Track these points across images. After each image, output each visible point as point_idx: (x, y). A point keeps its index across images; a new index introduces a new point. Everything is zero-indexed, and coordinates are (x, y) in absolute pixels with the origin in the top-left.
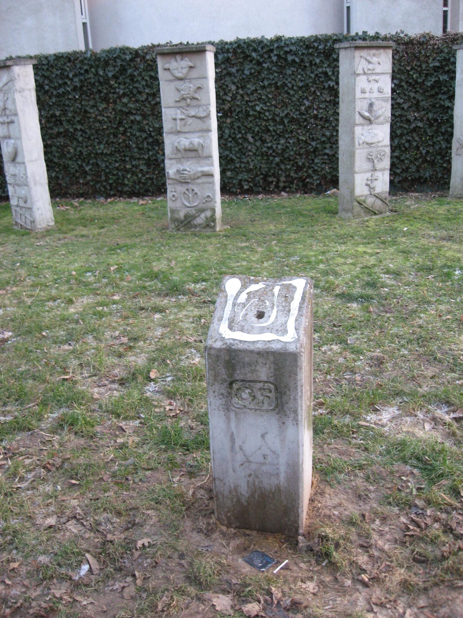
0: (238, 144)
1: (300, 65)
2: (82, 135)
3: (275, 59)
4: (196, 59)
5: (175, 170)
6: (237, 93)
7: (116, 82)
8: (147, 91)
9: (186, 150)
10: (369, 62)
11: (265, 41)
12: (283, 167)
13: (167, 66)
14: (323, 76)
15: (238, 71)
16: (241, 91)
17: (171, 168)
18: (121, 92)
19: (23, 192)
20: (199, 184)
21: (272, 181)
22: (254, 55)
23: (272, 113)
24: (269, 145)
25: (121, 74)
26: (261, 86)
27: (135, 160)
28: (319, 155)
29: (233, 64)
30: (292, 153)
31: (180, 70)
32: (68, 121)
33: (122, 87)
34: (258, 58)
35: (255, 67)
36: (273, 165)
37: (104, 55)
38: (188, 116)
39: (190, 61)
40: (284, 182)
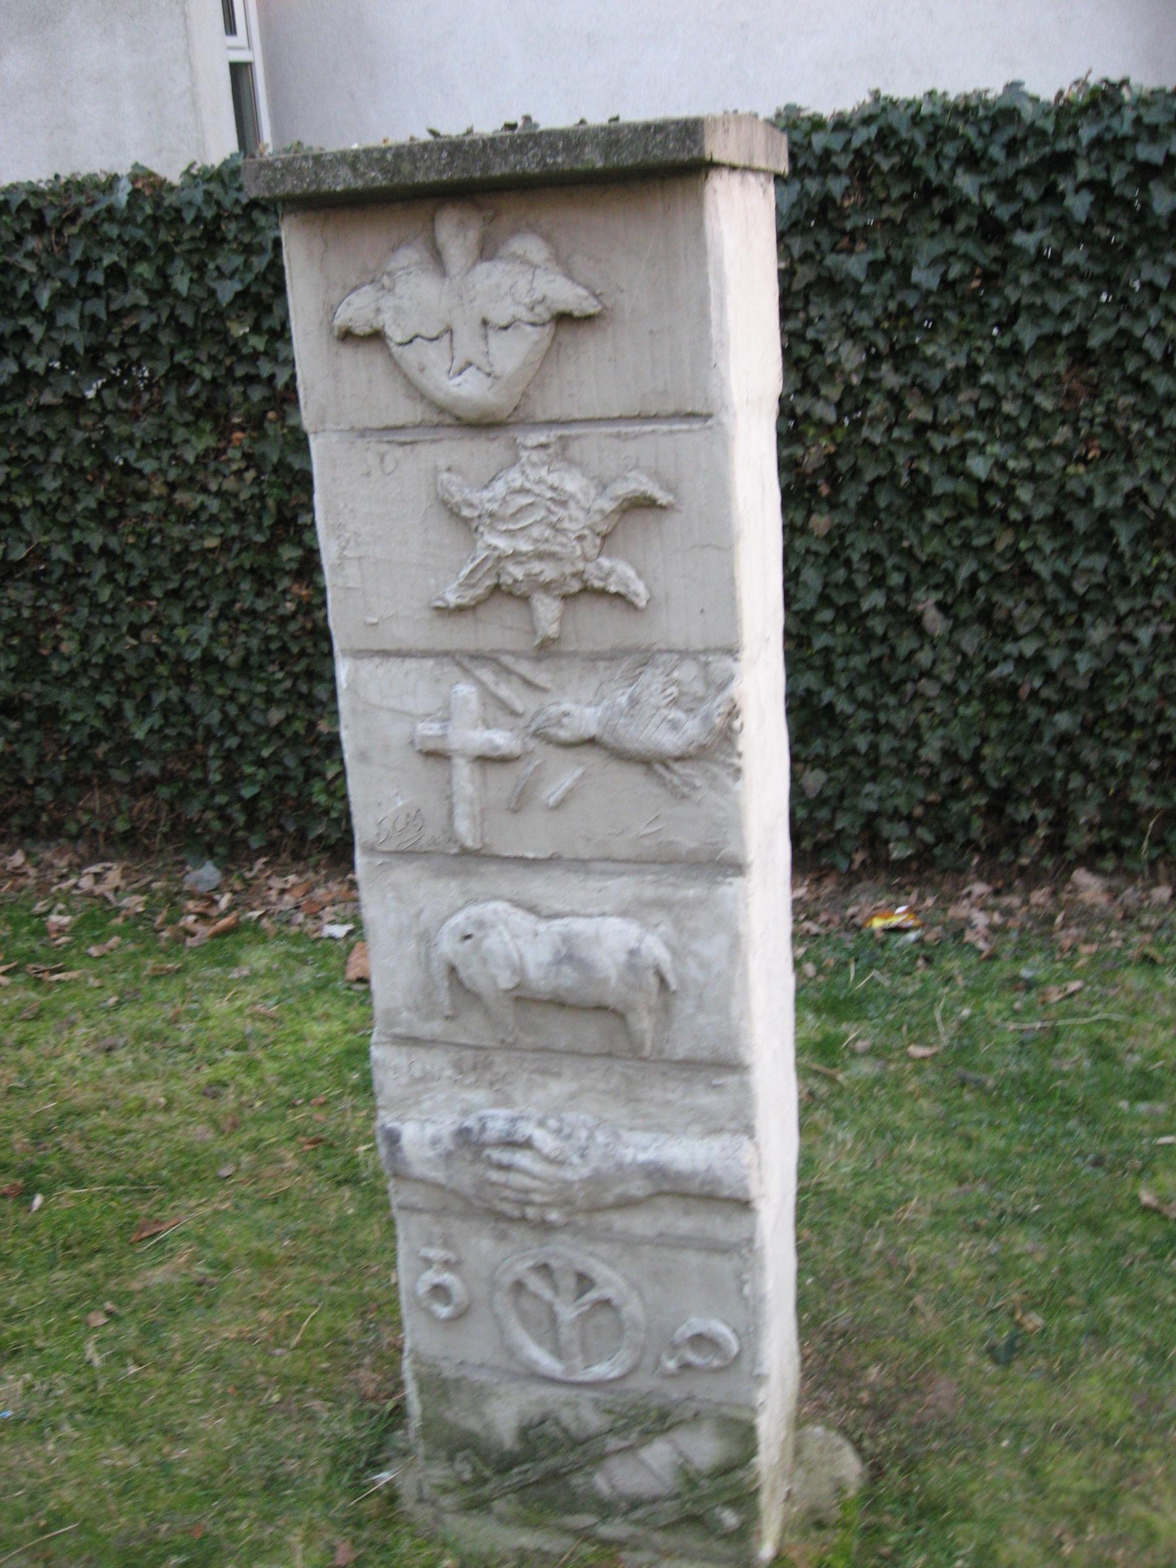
0: (868, 638)
2: (109, 578)
3: (1079, 205)
4: (614, 251)
5: (446, 1125)
6: (867, 382)
7: (256, 329)
9: (523, 998)
11: (1028, 112)
12: (1090, 755)
13: (357, 310)
15: (875, 270)
16: (890, 378)
20: (631, 1243)
21: (1032, 823)
22: (966, 183)
23: (1051, 489)
24: (1029, 648)
26: (999, 352)
29: (852, 236)
30: (1145, 693)
31: (467, 343)
32: (46, 511)
34: (990, 199)
35: (968, 247)
36: (1045, 747)
37: (198, 197)
40: (1091, 827)
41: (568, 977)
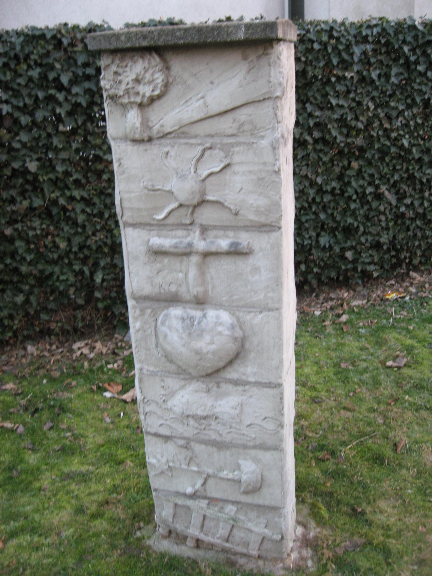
32: (54, 183)
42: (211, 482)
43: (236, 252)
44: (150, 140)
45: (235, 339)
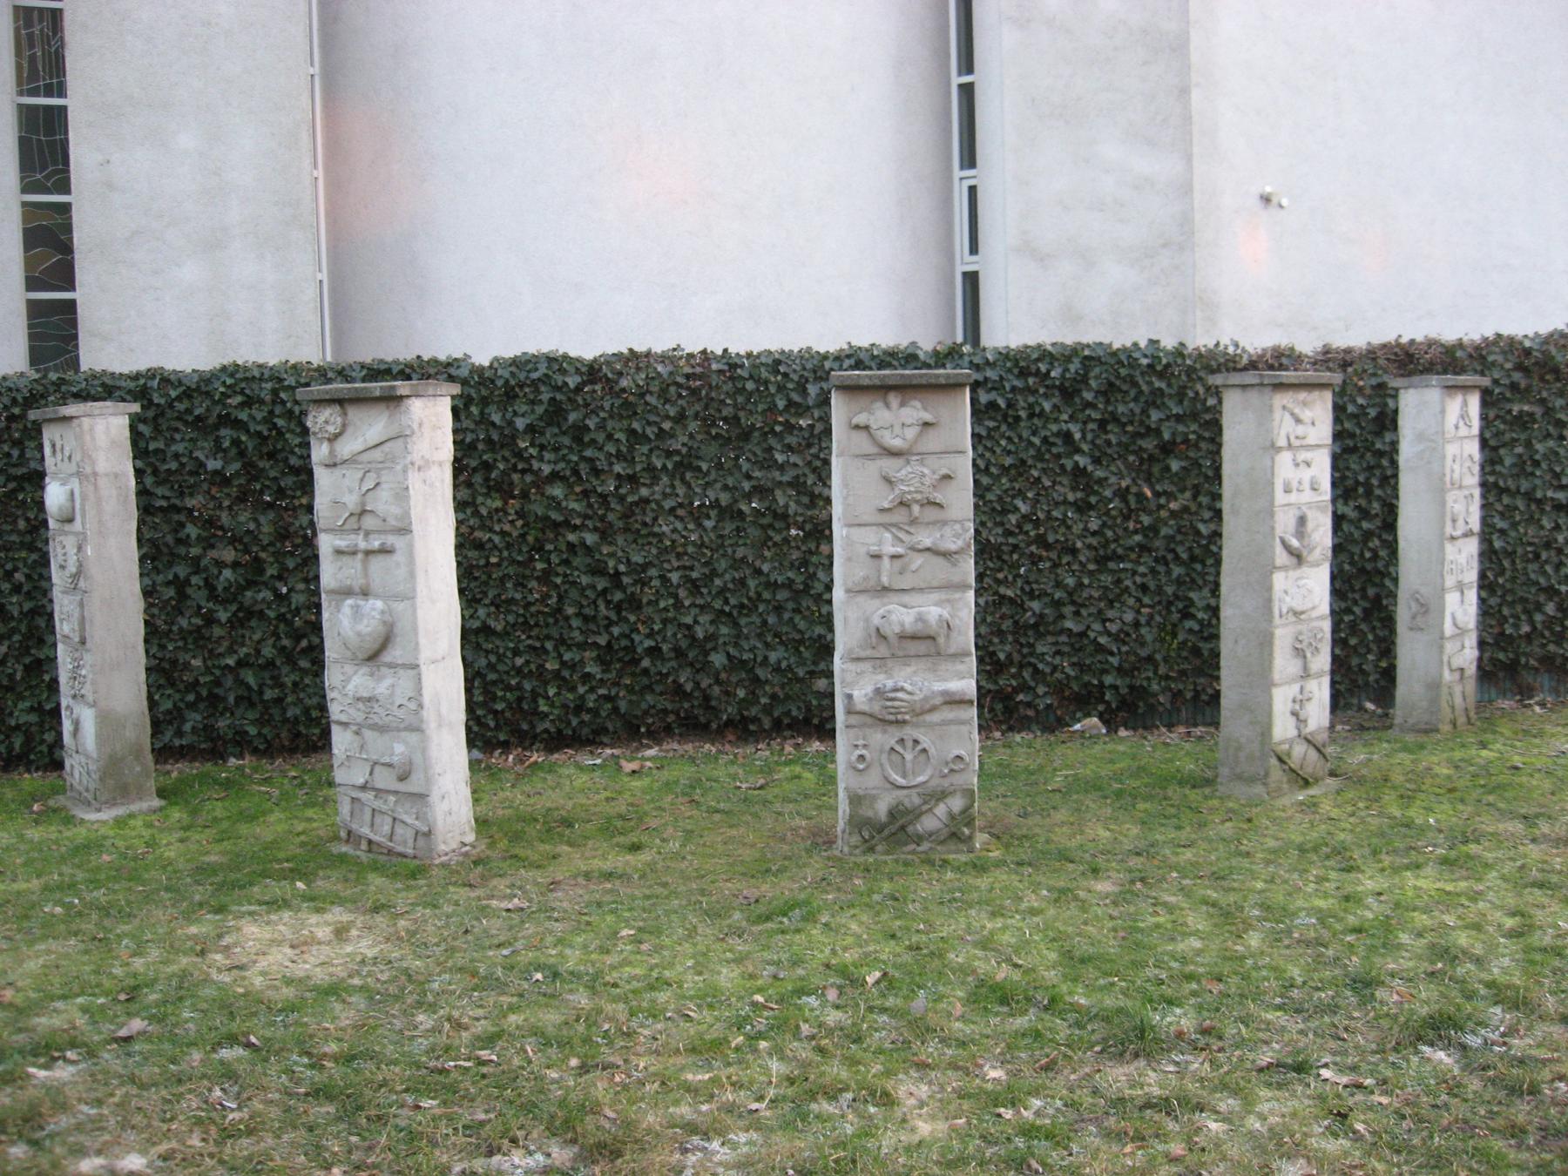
1: (1005, 416)
5: (869, 689)
7: (532, 445)
8: (618, 468)
9: (903, 637)
10: (1298, 421)
13: (861, 419)
14: (1059, 441)
17: (853, 683)
18: (547, 469)
19: (399, 748)
20: (932, 726)
25: (549, 425)
27: (569, 647)
28: (1049, 633)
31: (897, 429)
33: (547, 456)
38: (913, 549)
39: (925, 409)
41: (920, 626)
42: (378, 769)
43: (385, 551)
44: (335, 465)
45: (385, 623)
